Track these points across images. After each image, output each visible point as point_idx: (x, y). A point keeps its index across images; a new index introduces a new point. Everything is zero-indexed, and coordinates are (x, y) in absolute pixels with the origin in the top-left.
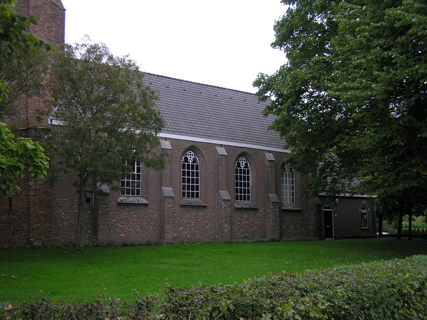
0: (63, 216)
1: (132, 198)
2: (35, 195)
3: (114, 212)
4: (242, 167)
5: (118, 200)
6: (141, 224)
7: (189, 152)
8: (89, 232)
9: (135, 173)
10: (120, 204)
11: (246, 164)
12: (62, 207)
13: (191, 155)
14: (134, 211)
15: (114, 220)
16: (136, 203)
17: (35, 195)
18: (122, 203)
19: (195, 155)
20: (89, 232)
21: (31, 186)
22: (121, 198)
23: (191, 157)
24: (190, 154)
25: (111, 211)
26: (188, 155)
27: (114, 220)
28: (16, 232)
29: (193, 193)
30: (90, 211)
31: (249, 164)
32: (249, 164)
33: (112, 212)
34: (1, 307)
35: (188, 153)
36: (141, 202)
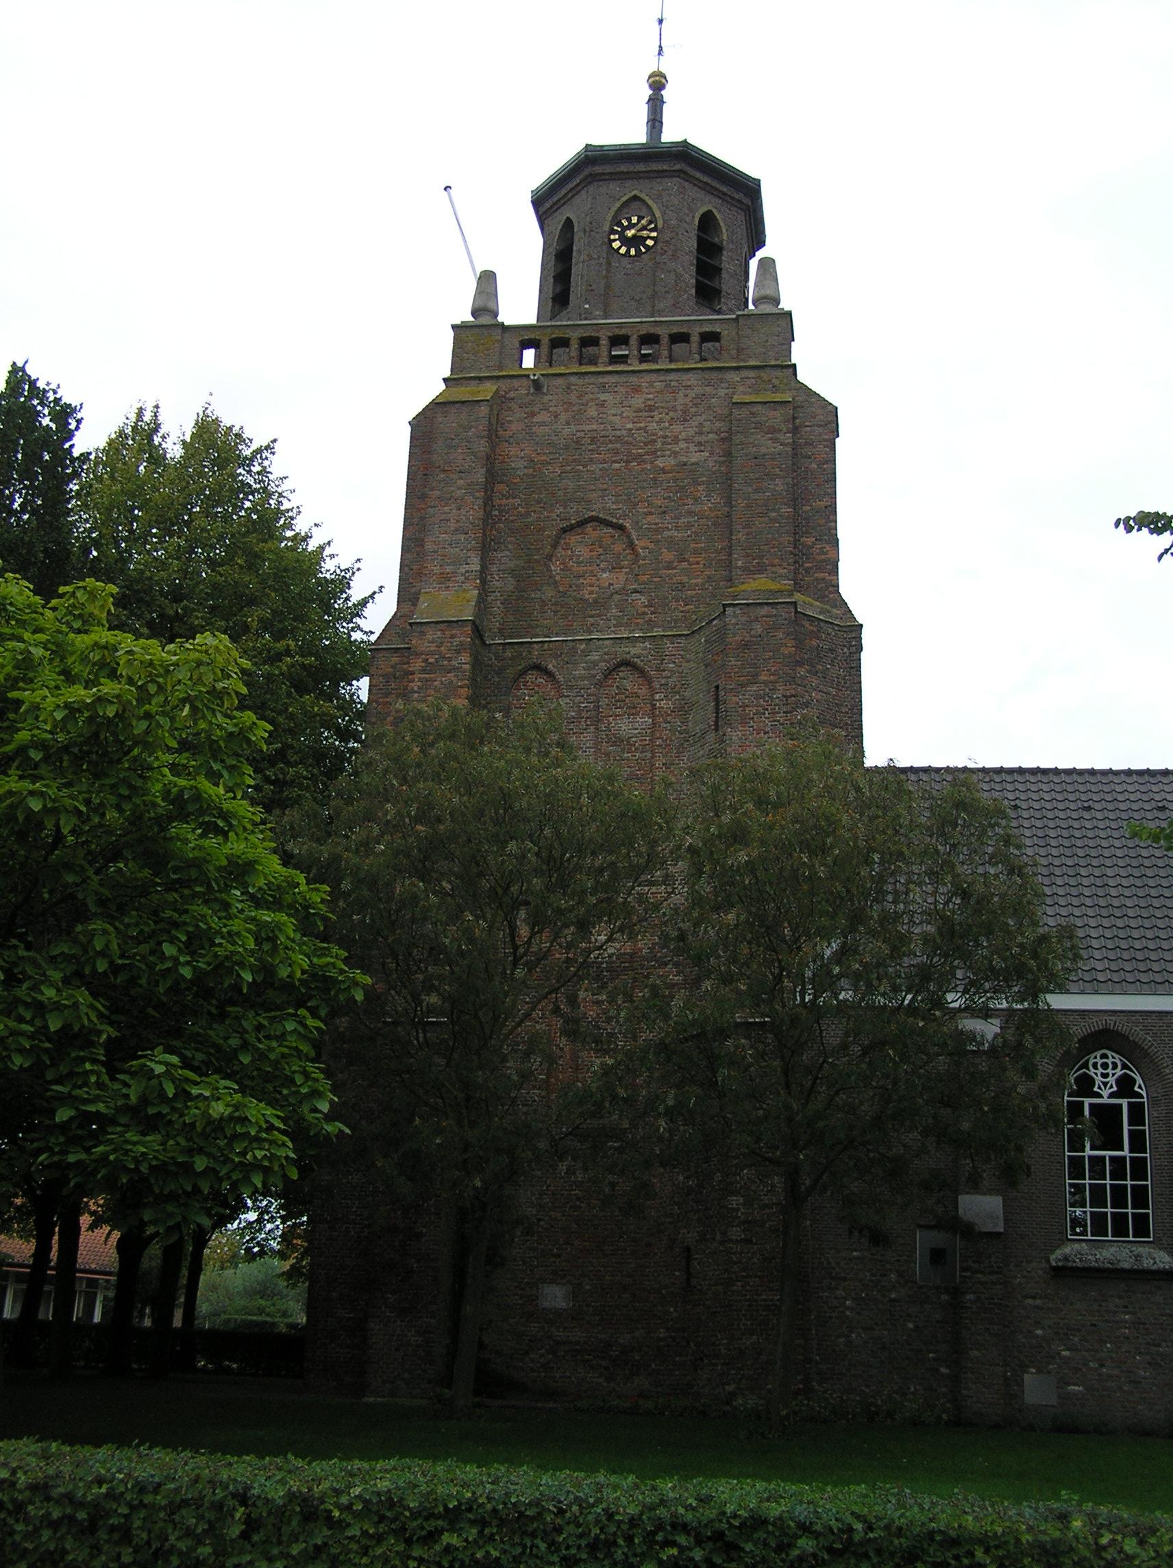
0: (848, 1313)
1: (1112, 1250)
2: (748, 1241)
3: (1038, 1302)
4: (1105, 1093)
5: (1053, 1257)
6: (1153, 1349)
7: (1098, 1054)
8: (943, 1370)
9: (1126, 1153)
10: (1063, 1273)
11: (1125, 1086)
12: (844, 1279)
13: (1105, 1066)
14: (1120, 1297)
15: (1039, 1332)
16: (1126, 1266)
17: (748, 1241)
18: (1064, 1268)
19: (1124, 1066)
20: (943, 1370)
21: (733, 1209)
22: (1067, 1250)
23: (1105, 1076)
24: (1100, 1062)
25: (1026, 1297)
26: (1115, 1066)
27: (1039, 1332)
28: (701, 1359)
29: (1120, 1221)
30: (945, 1297)
31: (1139, 1080)
32: (1139, 1080)
33: (1030, 1301)
34: (3, 1474)
35: (1095, 1058)
36: (1147, 1263)
